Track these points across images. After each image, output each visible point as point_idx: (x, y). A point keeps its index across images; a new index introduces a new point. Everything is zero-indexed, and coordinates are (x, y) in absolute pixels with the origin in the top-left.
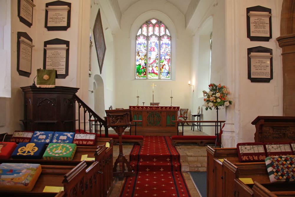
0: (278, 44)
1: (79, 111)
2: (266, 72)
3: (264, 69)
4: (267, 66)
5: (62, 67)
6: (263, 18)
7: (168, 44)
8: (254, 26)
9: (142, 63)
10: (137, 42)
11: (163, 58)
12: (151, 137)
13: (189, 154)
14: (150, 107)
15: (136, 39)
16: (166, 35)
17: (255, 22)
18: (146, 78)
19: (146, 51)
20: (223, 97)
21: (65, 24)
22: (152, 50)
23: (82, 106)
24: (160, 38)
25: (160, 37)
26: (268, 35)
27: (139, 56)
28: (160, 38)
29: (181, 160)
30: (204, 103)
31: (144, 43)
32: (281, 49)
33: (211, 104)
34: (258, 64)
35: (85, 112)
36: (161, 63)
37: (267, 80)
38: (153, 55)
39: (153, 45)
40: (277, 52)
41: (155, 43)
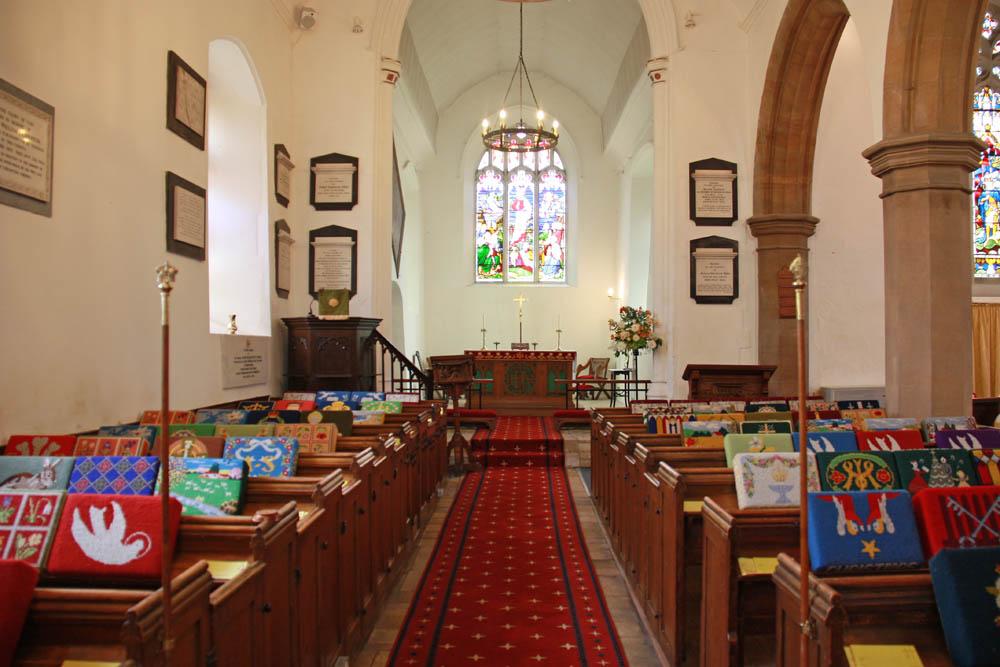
1: (381, 357)
5: (345, 278)
6: (720, 183)
7: (559, 192)
9: (493, 241)
10: (479, 187)
11: (546, 227)
12: (513, 418)
13: (581, 438)
14: (511, 353)
15: (477, 180)
16: (552, 166)
18: (501, 280)
19: (501, 211)
20: (644, 332)
21: (348, 199)
22: (517, 207)
23: (387, 351)
24: (537, 175)
25: (539, 172)
27: (485, 222)
28: (537, 175)
29: (566, 450)
30: (610, 342)
31: (498, 191)
32: (756, 239)
33: (622, 346)
34: (709, 271)
35: (393, 360)
36: (541, 242)
37: (727, 300)
38: (521, 221)
39: (520, 195)
40: (748, 246)
41: (524, 189)
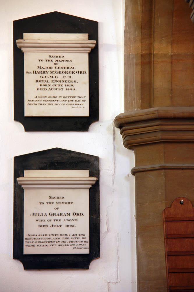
0: (120, 138)
2: (73, 233)
3: (69, 223)
4: (78, 214)
8: (37, 81)
17: (39, 67)
26: (84, 111)
32: (132, 154)
34: (47, 209)
